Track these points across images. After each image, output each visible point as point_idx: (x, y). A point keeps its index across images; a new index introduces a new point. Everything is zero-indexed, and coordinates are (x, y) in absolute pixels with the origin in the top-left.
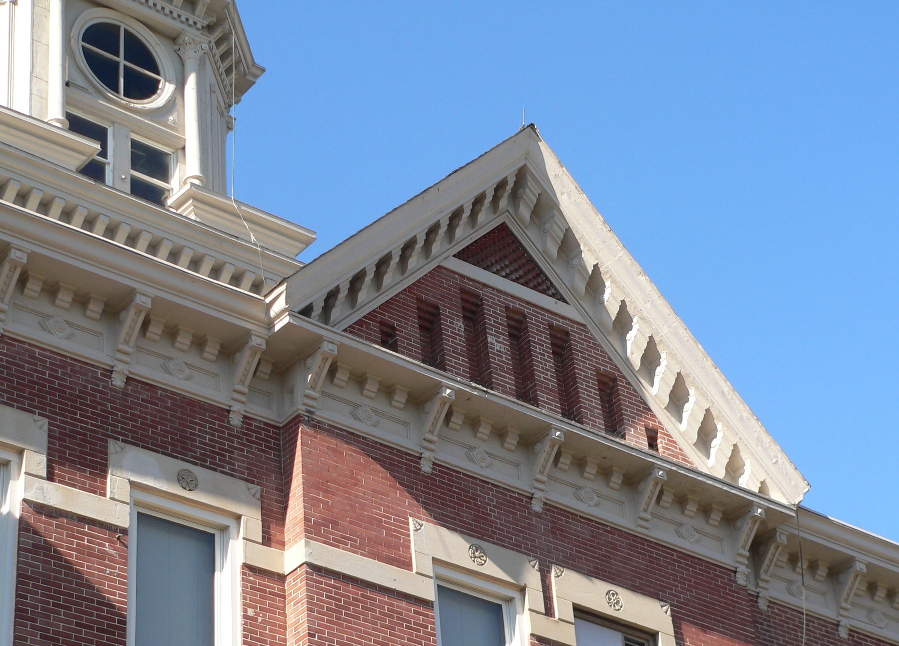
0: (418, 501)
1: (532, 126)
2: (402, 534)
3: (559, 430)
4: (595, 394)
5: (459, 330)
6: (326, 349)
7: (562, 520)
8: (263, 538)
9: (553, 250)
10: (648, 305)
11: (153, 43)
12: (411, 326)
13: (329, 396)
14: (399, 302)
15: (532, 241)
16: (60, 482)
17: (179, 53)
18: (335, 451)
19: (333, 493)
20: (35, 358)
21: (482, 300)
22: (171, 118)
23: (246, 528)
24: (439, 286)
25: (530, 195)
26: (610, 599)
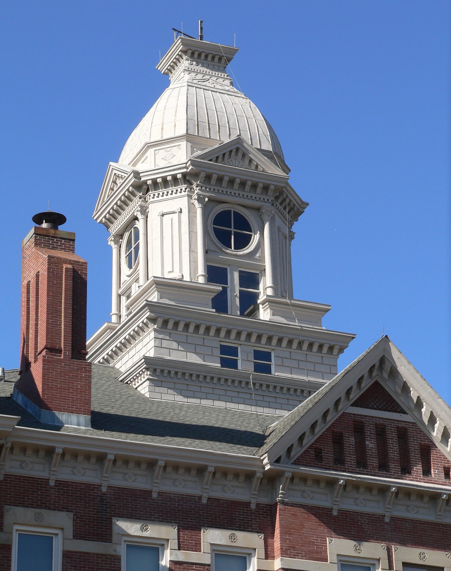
0: (331, 529)
1: (386, 336)
2: (323, 546)
3: (394, 487)
4: (418, 457)
5: (352, 442)
6: (287, 476)
7: (399, 523)
8: (265, 556)
9: (399, 391)
10: (443, 413)
11: (248, 215)
12: (329, 446)
13: (292, 490)
14: (324, 436)
15: (389, 387)
16: (183, 550)
17: (261, 216)
18: (294, 515)
19: (293, 534)
20: (172, 499)
21: (364, 423)
22: (258, 255)
23: (258, 554)
24: (343, 422)
25: (387, 367)
26: (420, 556)
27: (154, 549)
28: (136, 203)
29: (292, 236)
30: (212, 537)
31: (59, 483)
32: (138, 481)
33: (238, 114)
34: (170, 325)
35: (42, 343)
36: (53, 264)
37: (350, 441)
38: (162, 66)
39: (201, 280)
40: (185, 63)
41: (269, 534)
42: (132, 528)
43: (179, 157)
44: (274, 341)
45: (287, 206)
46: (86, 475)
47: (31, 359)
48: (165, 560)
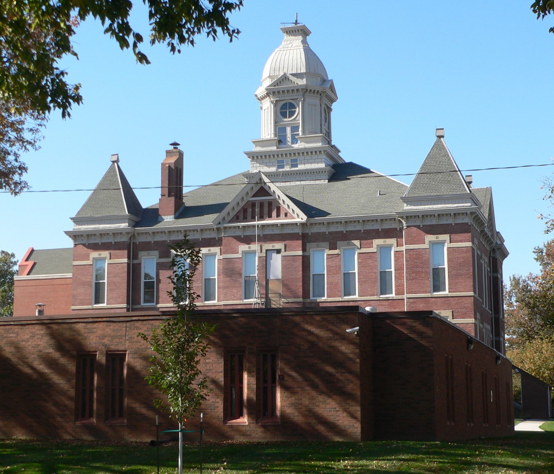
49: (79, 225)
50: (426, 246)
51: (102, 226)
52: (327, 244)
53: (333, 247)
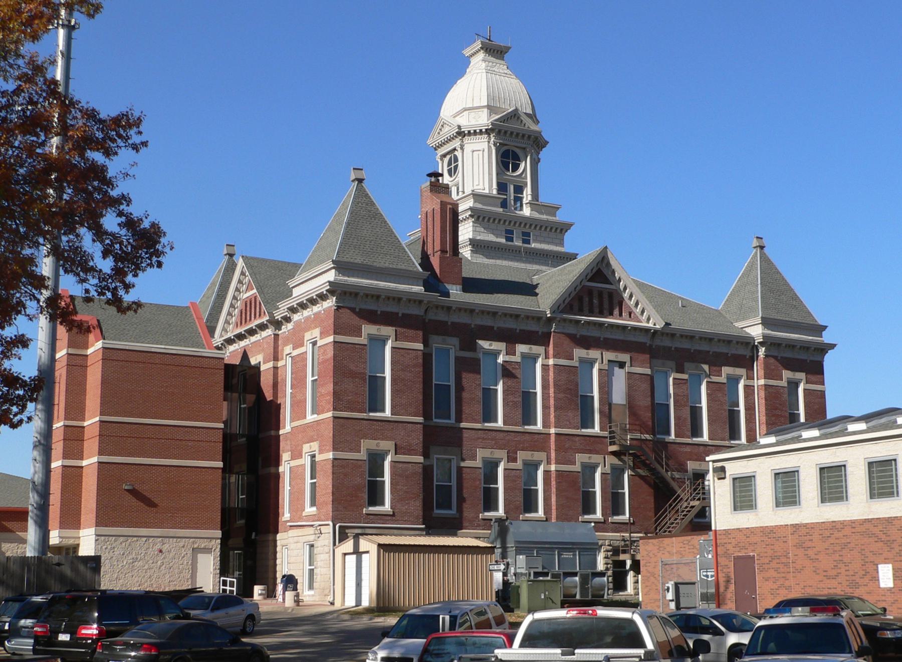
15: (605, 271)
25: (605, 262)
27: (496, 354)
28: (456, 143)
29: (539, 160)
30: (521, 348)
31: (452, 323)
32: (488, 322)
33: (515, 93)
34: (481, 219)
35: (438, 247)
36: (443, 205)
37: (586, 299)
38: (467, 52)
39: (495, 192)
40: (481, 55)
41: (546, 344)
42: (485, 344)
43: (483, 120)
44: (533, 227)
45: (537, 143)
46: (464, 319)
47: (430, 252)
48: (500, 360)
49: (344, 275)
50: (363, 340)
51: (382, 284)
52: (672, 364)
53: (680, 370)
